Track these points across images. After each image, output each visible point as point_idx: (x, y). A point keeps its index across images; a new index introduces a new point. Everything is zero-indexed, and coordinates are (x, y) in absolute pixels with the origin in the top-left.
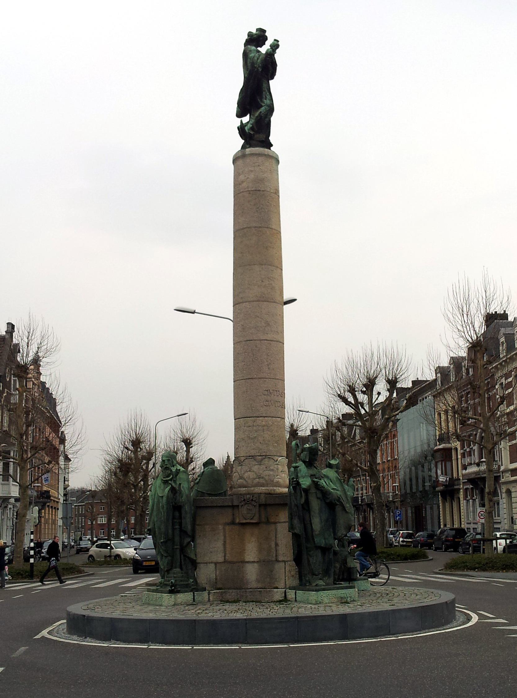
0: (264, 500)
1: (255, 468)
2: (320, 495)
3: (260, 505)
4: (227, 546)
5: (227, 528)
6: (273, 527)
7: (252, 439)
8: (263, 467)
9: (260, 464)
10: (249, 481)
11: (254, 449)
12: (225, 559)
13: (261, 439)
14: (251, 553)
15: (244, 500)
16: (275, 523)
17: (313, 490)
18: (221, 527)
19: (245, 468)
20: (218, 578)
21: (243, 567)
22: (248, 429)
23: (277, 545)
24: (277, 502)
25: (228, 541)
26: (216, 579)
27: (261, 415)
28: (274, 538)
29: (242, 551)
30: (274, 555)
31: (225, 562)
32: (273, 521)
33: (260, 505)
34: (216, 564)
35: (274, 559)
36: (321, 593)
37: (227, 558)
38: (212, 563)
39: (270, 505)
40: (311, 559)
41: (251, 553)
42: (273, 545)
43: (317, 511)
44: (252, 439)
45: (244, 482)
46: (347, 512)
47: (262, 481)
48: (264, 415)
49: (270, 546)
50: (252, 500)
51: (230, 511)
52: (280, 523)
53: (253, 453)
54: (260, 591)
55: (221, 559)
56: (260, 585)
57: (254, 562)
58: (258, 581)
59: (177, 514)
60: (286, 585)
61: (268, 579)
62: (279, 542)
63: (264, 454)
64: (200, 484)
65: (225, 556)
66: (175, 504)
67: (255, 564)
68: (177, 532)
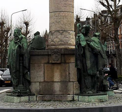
0: (63, 52)
1: (59, 37)
2: (90, 50)
3: (61, 54)
4: (46, 74)
5: (45, 65)
6: (68, 65)
7: (58, 22)
8: (62, 36)
9: (62, 35)
10: (56, 43)
11: (59, 27)
12: (44, 80)
13: (62, 22)
14: (57, 77)
15: (54, 52)
16: (69, 63)
17: (87, 47)
18: (42, 65)
19: (54, 36)
20: (41, 89)
21: (53, 84)
22: (56, 17)
23: (69, 74)
24: (70, 53)
25: (46, 72)
26: (40, 90)
27: (62, 11)
28: (68, 70)
29: (53, 77)
30: (68, 79)
31: (44, 81)
32: (67, 62)
33: (61, 54)
34: (40, 82)
35: (68, 80)
36: (91, 97)
37: (45, 80)
38: (38, 82)
39: (66, 54)
40: (86, 81)
41: (57, 77)
42: (68, 74)
44: (58, 22)
45: (54, 43)
46: (103, 58)
47: (62, 43)
48: (64, 11)
49: (66, 74)
50: (58, 52)
51: (47, 57)
52: (71, 63)
53: (58, 29)
54: (61, 96)
55: (42, 80)
56: (61, 93)
57: (58, 82)
58: (60, 91)
59: (21, 58)
60: (73, 93)
61: (65, 90)
62: (71, 72)
63: (64, 30)
64: (33, 44)
65: (44, 79)
66: (21, 53)
67: (59, 83)
68: (21, 67)
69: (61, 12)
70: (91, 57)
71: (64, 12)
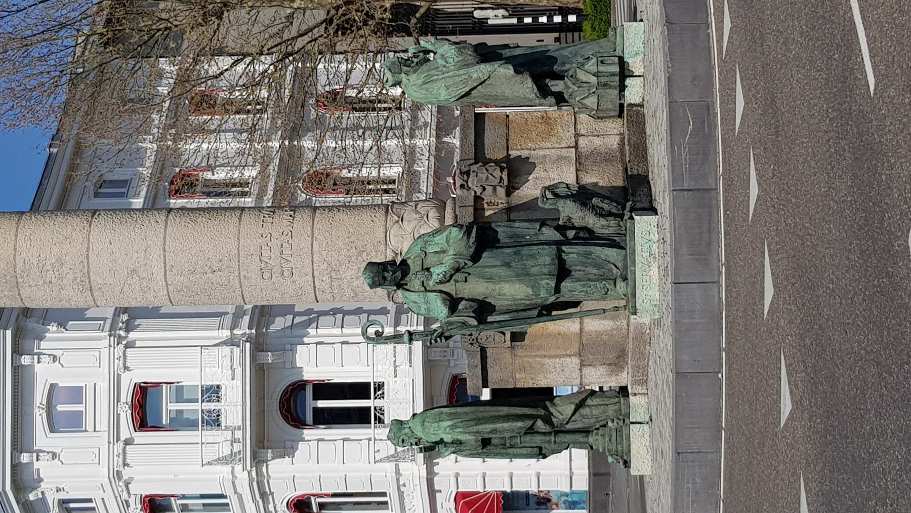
43: (491, 286)
48: (310, 277)
69: (317, 287)
70: (490, 279)
71: (314, 277)
